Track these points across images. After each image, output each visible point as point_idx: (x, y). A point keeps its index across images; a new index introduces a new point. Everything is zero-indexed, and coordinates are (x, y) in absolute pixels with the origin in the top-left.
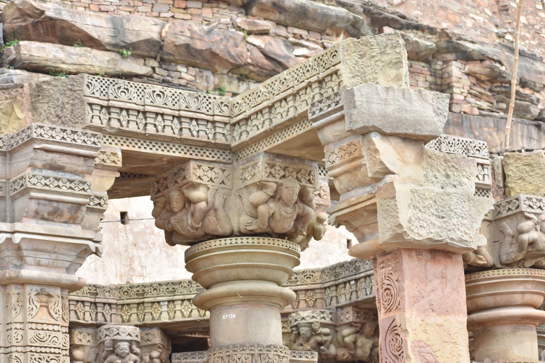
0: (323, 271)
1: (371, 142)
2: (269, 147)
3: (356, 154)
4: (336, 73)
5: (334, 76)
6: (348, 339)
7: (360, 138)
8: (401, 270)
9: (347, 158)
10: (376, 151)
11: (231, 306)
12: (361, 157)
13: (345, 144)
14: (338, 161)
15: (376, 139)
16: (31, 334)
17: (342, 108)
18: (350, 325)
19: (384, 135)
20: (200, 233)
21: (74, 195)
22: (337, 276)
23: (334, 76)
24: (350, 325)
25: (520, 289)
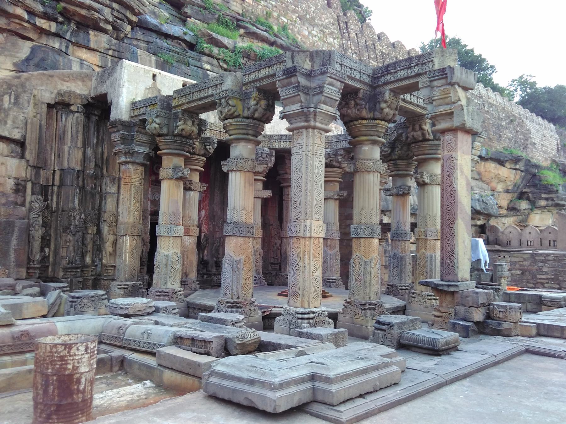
0: (332, 136)
1: (455, 88)
2: (392, 87)
3: (448, 92)
4: (432, 61)
5: (431, 63)
6: (340, 160)
7: (450, 86)
8: (457, 137)
9: (442, 93)
10: (457, 92)
11: (366, 145)
12: (450, 93)
13: (442, 88)
14: (437, 95)
15: (457, 87)
16: (315, 148)
17: (446, 74)
18: (341, 155)
19: (459, 86)
20: (359, 117)
21: (335, 96)
22: (337, 138)
23: (431, 63)
24: (341, 155)
25: (428, 148)
